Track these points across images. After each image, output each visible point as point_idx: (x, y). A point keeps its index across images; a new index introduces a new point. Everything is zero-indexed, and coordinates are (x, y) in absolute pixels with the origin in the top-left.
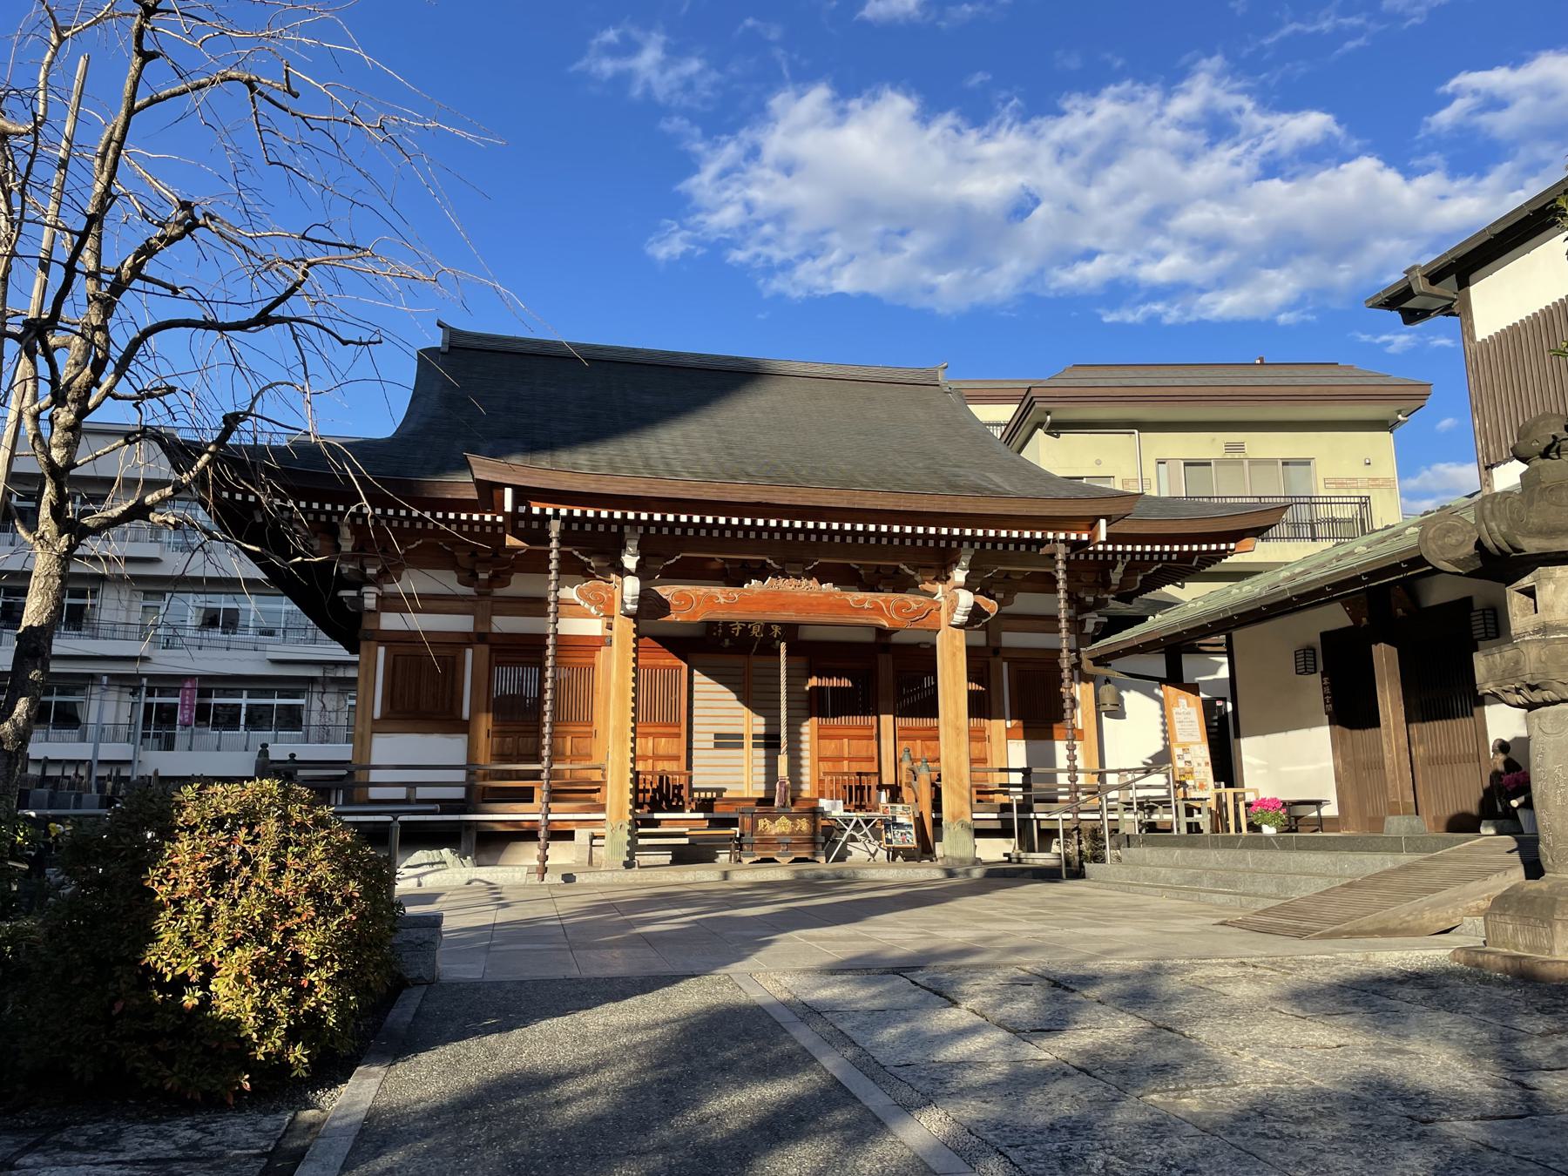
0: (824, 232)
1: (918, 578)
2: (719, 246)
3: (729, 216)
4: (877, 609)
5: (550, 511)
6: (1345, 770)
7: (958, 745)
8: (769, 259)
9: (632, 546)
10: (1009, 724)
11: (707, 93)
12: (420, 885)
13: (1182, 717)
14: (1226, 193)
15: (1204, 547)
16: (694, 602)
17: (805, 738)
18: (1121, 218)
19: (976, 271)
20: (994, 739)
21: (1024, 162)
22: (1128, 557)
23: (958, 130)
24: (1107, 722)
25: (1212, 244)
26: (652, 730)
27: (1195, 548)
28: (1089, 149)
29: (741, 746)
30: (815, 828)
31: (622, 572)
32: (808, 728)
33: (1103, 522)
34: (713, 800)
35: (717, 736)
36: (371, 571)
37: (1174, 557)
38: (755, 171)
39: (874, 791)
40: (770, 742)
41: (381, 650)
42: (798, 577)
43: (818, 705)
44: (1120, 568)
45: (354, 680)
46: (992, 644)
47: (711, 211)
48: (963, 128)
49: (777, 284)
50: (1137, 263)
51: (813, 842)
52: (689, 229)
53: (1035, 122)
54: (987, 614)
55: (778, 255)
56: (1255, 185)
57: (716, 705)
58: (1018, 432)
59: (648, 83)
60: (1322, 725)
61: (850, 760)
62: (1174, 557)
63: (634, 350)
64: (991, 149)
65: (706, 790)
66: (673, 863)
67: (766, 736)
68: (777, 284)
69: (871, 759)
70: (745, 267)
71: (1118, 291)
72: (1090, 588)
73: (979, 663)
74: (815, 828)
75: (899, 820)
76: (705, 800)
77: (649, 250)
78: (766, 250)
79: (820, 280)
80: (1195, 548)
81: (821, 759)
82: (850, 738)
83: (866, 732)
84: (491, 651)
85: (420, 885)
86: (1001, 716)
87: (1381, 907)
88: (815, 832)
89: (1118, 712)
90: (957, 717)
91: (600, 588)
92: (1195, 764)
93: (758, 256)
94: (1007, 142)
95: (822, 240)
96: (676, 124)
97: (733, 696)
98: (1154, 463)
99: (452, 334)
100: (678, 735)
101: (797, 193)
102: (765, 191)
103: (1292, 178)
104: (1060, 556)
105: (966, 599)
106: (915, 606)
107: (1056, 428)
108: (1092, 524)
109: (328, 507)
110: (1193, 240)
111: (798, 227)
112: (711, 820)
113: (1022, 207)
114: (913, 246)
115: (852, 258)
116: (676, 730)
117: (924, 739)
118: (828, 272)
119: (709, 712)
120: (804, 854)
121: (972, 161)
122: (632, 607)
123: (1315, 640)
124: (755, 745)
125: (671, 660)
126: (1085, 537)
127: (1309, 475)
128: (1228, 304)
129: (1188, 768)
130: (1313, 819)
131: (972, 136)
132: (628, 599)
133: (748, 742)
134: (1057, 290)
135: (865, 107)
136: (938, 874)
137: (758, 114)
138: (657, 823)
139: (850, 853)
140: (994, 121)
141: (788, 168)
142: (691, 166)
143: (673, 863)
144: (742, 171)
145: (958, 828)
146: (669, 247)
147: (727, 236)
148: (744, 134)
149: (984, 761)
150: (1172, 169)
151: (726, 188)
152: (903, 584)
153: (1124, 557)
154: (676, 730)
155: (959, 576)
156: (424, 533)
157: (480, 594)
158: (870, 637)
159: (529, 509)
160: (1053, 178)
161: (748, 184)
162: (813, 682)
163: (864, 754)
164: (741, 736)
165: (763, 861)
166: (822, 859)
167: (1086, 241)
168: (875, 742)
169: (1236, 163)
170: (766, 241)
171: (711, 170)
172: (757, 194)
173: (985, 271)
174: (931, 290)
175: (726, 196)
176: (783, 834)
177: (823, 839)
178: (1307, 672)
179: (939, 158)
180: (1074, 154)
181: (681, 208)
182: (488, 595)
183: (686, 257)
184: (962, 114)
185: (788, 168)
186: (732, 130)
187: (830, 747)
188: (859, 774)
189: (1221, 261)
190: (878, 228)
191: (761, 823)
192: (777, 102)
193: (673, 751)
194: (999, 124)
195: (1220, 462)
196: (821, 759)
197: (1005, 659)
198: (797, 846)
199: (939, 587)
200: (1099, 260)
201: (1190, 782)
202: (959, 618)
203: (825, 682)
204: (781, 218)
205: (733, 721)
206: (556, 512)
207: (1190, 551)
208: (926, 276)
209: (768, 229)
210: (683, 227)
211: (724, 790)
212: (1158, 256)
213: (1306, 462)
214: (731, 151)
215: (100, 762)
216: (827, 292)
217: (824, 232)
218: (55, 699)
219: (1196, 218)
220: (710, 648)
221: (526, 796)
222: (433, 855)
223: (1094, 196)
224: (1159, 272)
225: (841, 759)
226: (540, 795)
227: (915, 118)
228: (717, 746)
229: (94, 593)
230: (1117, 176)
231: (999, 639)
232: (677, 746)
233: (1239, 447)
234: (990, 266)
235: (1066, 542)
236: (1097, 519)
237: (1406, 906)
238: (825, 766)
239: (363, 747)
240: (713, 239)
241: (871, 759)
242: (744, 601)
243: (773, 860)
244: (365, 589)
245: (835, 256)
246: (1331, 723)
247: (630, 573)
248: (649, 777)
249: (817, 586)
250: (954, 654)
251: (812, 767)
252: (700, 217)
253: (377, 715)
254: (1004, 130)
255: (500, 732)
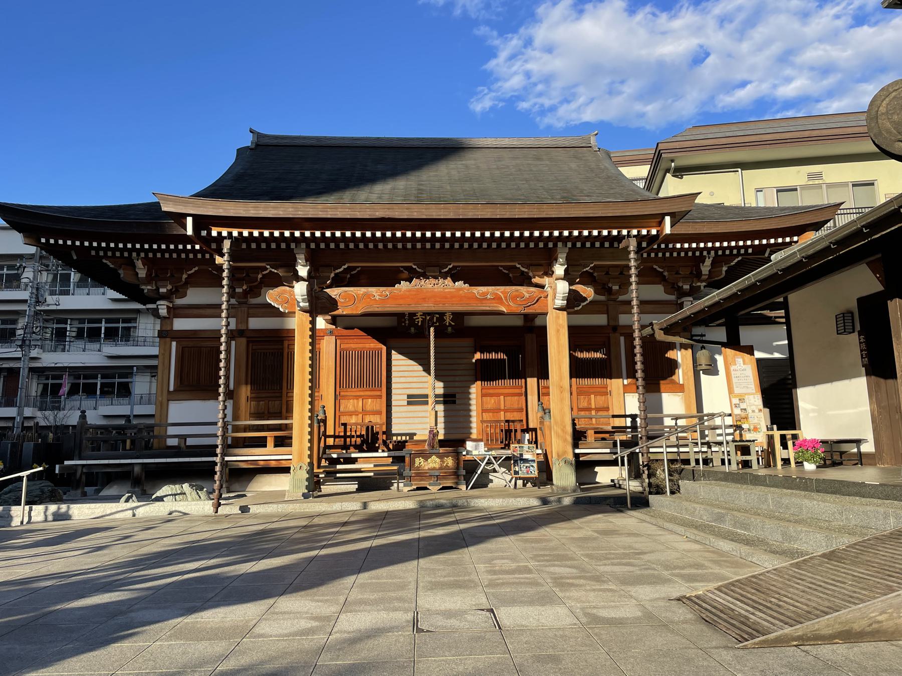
0: (576, 85)
1: (531, 274)
2: (512, 100)
3: (515, 82)
4: (498, 299)
5: (225, 234)
6: (880, 413)
7: (562, 400)
8: (542, 105)
9: (301, 259)
10: (626, 382)
11: (499, 9)
12: (134, 515)
13: (738, 374)
14: (831, 37)
15: (772, 241)
16: (353, 299)
17: (473, 396)
18: (762, 59)
19: (670, 101)
20: (614, 393)
21: (698, 30)
22: (713, 253)
23: (654, 15)
24: (704, 378)
25: (825, 70)
26: (362, 393)
27: (764, 242)
28: (742, 16)
29: (426, 403)
30: (458, 464)
31: (299, 279)
32: (475, 389)
33: (668, 219)
34: (406, 441)
35: (409, 396)
36: (163, 290)
37: (750, 251)
38: (530, 52)
39: (519, 433)
40: (448, 399)
41: (174, 344)
42: (436, 278)
43: (488, 372)
44: (708, 262)
45: (155, 367)
46: (612, 323)
47: (506, 80)
48: (658, 13)
49: (548, 120)
50: (775, 86)
51: (456, 474)
52: (494, 91)
53: (704, 4)
54: (585, 299)
55: (547, 102)
56: (852, 30)
57: (409, 375)
58: (653, 181)
59: (464, 6)
60: (859, 376)
61: (506, 411)
62: (750, 251)
63: (378, 138)
64: (677, 24)
65: (401, 435)
66: (359, 490)
67: (445, 395)
68: (548, 120)
69: (520, 410)
70: (528, 112)
71: (762, 104)
72: (685, 279)
73: (578, 337)
74: (458, 464)
75: (525, 456)
76: (399, 442)
77: (471, 107)
78: (541, 100)
79: (574, 116)
80: (764, 242)
81: (484, 411)
82: (506, 395)
83: (517, 391)
84: (248, 343)
85: (134, 515)
86: (619, 376)
87: (852, 600)
88: (458, 468)
89: (712, 370)
90: (561, 379)
91: (285, 291)
92: (749, 411)
93: (535, 104)
94: (686, 18)
95: (573, 91)
96: (483, 30)
97: (420, 368)
98: (754, 192)
99: (259, 136)
100: (380, 397)
101: (556, 64)
102: (538, 64)
103: (876, 23)
104: (632, 248)
105: (563, 287)
106: (527, 295)
107: (680, 172)
108: (661, 223)
109: (129, 246)
110: (812, 69)
111: (558, 84)
112: (394, 458)
113: (699, 57)
114: (630, 88)
115: (592, 100)
116: (378, 393)
117: (596, 394)
118: (579, 110)
119: (402, 380)
120: (449, 483)
121: (664, 33)
122: (306, 305)
123: (853, 305)
124: (437, 402)
125: (373, 344)
126: (654, 232)
127: (874, 191)
128: (834, 106)
129: (743, 414)
130: (854, 454)
131: (664, 17)
132: (299, 298)
133: (431, 400)
134: (724, 107)
135: (595, 7)
136: (535, 502)
137: (532, 18)
138: (354, 461)
139: (491, 481)
140: (678, 6)
141: (549, 49)
142: (492, 53)
143: (359, 490)
144: (523, 54)
145: (562, 464)
146: (482, 105)
147: (516, 94)
148: (522, 30)
149: (607, 409)
150: (796, 25)
151: (513, 65)
152: (525, 280)
153: (709, 253)
154: (378, 393)
155: (559, 270)
156: (195, 262)
157: (240, 303)
158: (519, 322)
159: (209, 233)
160: (716, 38)
161: (526, 61)
162: (478, 356)
163: (516, 407)
164: (426, 396)
165: (418, 489)
166: (463, 487)
167: (740, 76)
168: (523, 398)
169: (837, 17)
170: (540, 95)
171: (503, 55)
172: (530, 66)
173: (676, 101)
174: (642, 115)
175: (513, 70)
176: (434, 469)
177: (464, 472)
178: (845, 332)
179: (642, 33)
180: (731, 21)
181: (488, 79)
182: (246, 303)
183: (493, 109)
184: (657, 5)
185: (549, 49)
186: (515, 31)
187: (491, 402)
188: (507, 421)
189: (829, 82)
190: (607, 80)
191: (417, 460)
192: (541, 10)
193: (377, 408)
194: (681, 7)
195: (804, 187)
196: (484, 411)
197: (622, 334)
198: (444, 478)
199: (546, 281)
200: (749, 86)
201: (745, 426)
202: (560, 302)
203: (486, 356)
204: (547, 79)
205: (421, 385)
206: (230, 234)
207: (760, 245)
208: (639, 107)
209: (540, 87)
210: (490, 90)
211: (415, 434)
212: (789, 80)
213: (871, 184)
214: (515, 42)
215: (135, 416)
216: (577, 122)
217: (576, 85)
218: (117, 380)
219: (813, 54)
220: (399, 332)
221: (261, 443)
222: (176, 488)
223: (745, 47)
224: (789, 90)
225: (499, 410)
226: (270, 442)
227: (626, 10)
228: (409, 403)
229: (135, 320)
230: (760, 33)
231: (617, 319)
232: (381, 405)
233: (819, 175)
234: (678, 97)
235: (639, 237)
236: (663, 216)
237: (879, 602)
238: (487, 417)
239: (163, 410)
240: (508, 95)
241: (520, 410)
242: (394, 297)
243: (426, 488)
244: (158, 303)
245: (582, 100)
246: (867, 374)
247: (303, 279)
248: (354, 427)
249: (451, 283)
250: (558, 331)
251: (477, 416)
252: (499, 84)
253: (172, 388)
254: (684, 10)
255: (255, 397)
